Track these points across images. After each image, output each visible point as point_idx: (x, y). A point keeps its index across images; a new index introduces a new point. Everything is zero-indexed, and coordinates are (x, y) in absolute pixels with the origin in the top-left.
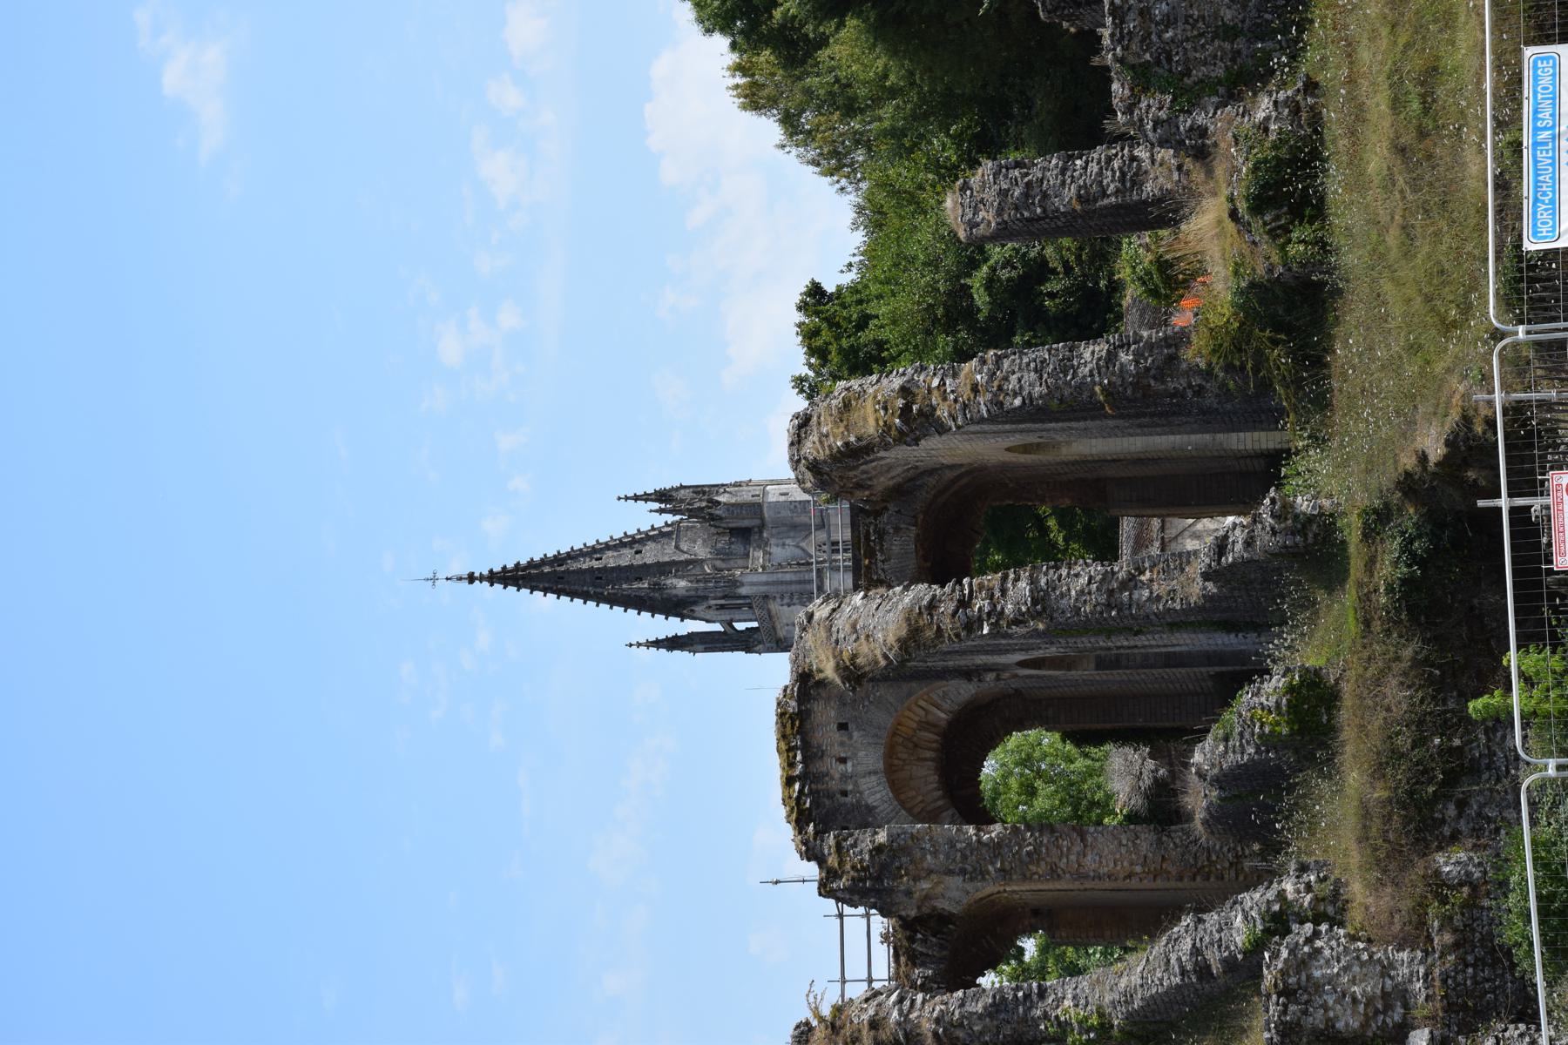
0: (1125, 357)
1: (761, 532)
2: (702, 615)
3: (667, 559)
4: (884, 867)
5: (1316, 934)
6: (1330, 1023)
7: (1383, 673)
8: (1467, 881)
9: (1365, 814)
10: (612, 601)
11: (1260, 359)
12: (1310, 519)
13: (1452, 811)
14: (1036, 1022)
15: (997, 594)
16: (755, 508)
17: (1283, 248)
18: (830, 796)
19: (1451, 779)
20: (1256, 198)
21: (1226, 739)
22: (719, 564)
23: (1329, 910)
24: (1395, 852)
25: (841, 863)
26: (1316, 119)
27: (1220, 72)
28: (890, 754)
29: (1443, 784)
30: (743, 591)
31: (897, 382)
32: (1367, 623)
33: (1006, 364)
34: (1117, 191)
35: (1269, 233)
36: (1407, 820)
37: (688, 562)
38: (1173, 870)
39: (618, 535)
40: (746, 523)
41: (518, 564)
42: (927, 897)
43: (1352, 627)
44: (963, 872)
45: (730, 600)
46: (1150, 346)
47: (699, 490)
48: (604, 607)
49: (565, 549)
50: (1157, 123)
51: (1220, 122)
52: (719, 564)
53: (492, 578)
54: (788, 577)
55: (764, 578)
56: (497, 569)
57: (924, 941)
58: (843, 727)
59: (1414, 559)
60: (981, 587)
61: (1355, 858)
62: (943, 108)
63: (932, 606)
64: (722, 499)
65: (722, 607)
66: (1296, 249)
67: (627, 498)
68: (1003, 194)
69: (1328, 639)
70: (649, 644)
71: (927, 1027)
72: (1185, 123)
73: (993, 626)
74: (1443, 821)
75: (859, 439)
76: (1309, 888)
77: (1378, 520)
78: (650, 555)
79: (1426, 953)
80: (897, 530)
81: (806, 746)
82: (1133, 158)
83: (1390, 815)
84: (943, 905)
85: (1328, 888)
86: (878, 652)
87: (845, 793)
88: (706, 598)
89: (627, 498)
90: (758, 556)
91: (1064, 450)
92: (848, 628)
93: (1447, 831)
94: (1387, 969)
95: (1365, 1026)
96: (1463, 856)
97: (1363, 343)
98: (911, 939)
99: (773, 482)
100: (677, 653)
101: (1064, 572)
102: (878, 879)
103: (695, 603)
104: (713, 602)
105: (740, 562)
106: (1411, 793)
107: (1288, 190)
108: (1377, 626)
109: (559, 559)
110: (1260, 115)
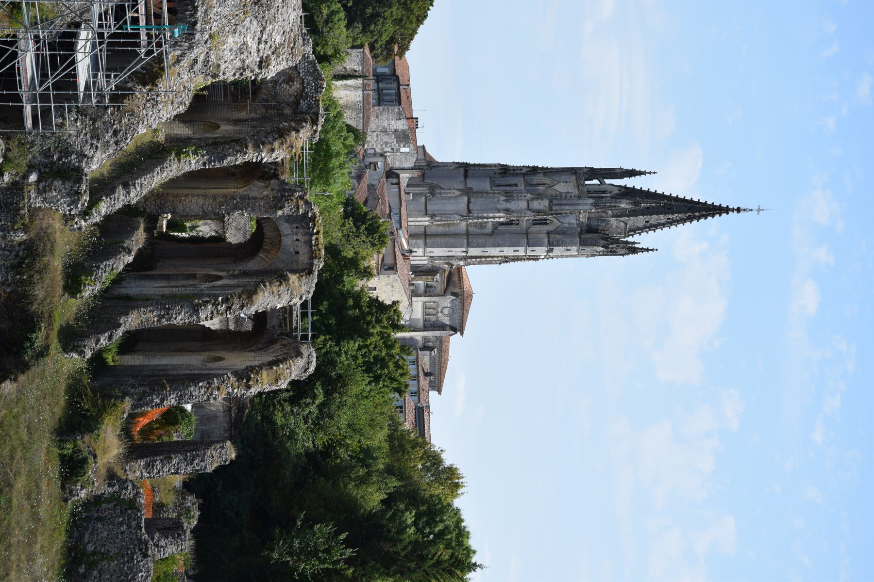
0: (158, 401)
1: (581, 231)
2: (615, 188)
3: (632, 218)
4: (280, 201)
5: (70, 211)
6: (64, 183)
7: (45, 299)
8: (15, 231)
9: (52, 251)
10: (663, 196)
11: (95, 405)
12: (72, 351)
13: (21, 253)
14: (207, 154)
15: (215, 312)
16: (583, 243)
17: (75, 446)
18: (302, 227)
19: (20, 264)
20: (85, 463)
21: (112, 269)
22: (604, 215)
23: (67, 219)
24: (41, 239)
25: (297, 202)
26: (63, 487)
27: (104, 506)
28: (280, 241)
29: (23, 263)
30: (591, 201)
31: (252, 390)
32: (50, 316)
33: (205, 398)
34: (155, 461)
35: (81, 451)
36: (36, 250)
37: (620, 216)
38: (170, 198)
39: (658, 231)
40: (589, 236)
41: (713, 217)
42: (266, 187)
43: (56, 315)
44: (249, 199)
45: (598, 196)
46: (147, 405)
47: (614, 253)
48: (667, 193)
49: (687, 224)
50: (126, 489)
51: (100, 487)
52: (604, 215)
53: (727, 210)
54: (567, 207)
55: (580, 207)
56: (724, 215)
57: (271, 169)
58: (297, 253)
59: (30, 340)
60: (222, 314)
61: (58, 235)
62: (343, 470)
63: (242, 307)
64: (601, 249)
65: (604, 192)
66: (70, 446)
67: (653, 250)
68: (203, 460)
69: (67, 309)
70: (644, 173)
71: (250, 150)
72: (116, 488)
73: (217, 300)
74: (24, 250)
75: (271, 368)
76: (76, 223)
77: (43, 353)
78: (641, 221)
79: (30, 206)
80: (274, 327)
81: (311, 246)
82: (149, 473)
83: (327, 22)
84: (261, 184)
85: (69, 223)
86: (268, 287)
87: (297, 228)
88: (612, 197)
89: (653, 250)
90: (583, 218)
91: (206, 357)
92: (282, 296)
93: (23, 247)
94: (45, 200)
95: (52, 182)
96: (17, 239)
98: (276, 170)
99: (575, 256)
100: (630, 168)
101: (187, 321)
102: (282, 196)
103: (618, 195)
104: (608, 195)
105: (593, 215)
106: (35, 259)
107: (73, 467)
108: (46, 315)
109: (691, 219)
110: (84, 491)
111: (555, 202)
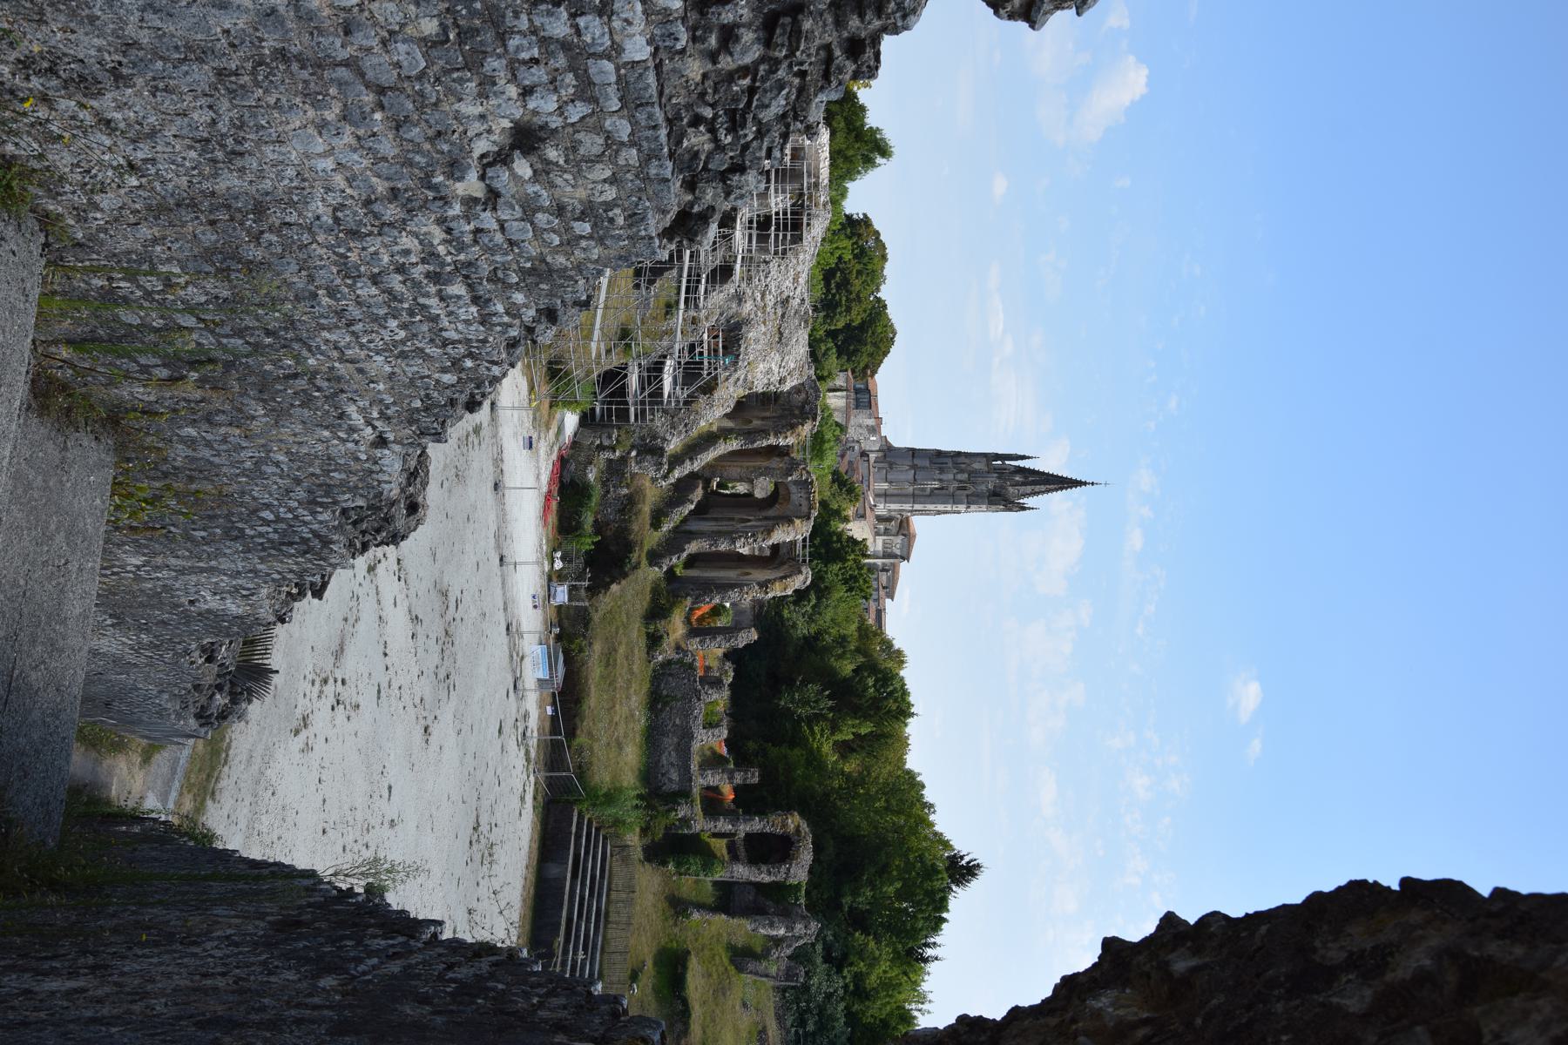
16: (991, 503)
23: (654, 480)
45: (1002, 472)
47: (1010, 510)
53: (1085, 484)
62: (827, 650)
69: (652, 538)
77: (637, 567)
97: (641, 604)
107: (654, 640)
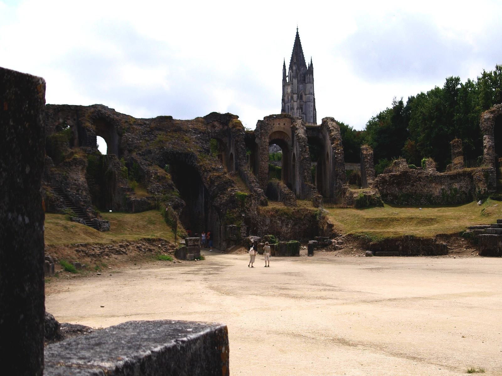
53: (297, 33)
111: (294, 92)
